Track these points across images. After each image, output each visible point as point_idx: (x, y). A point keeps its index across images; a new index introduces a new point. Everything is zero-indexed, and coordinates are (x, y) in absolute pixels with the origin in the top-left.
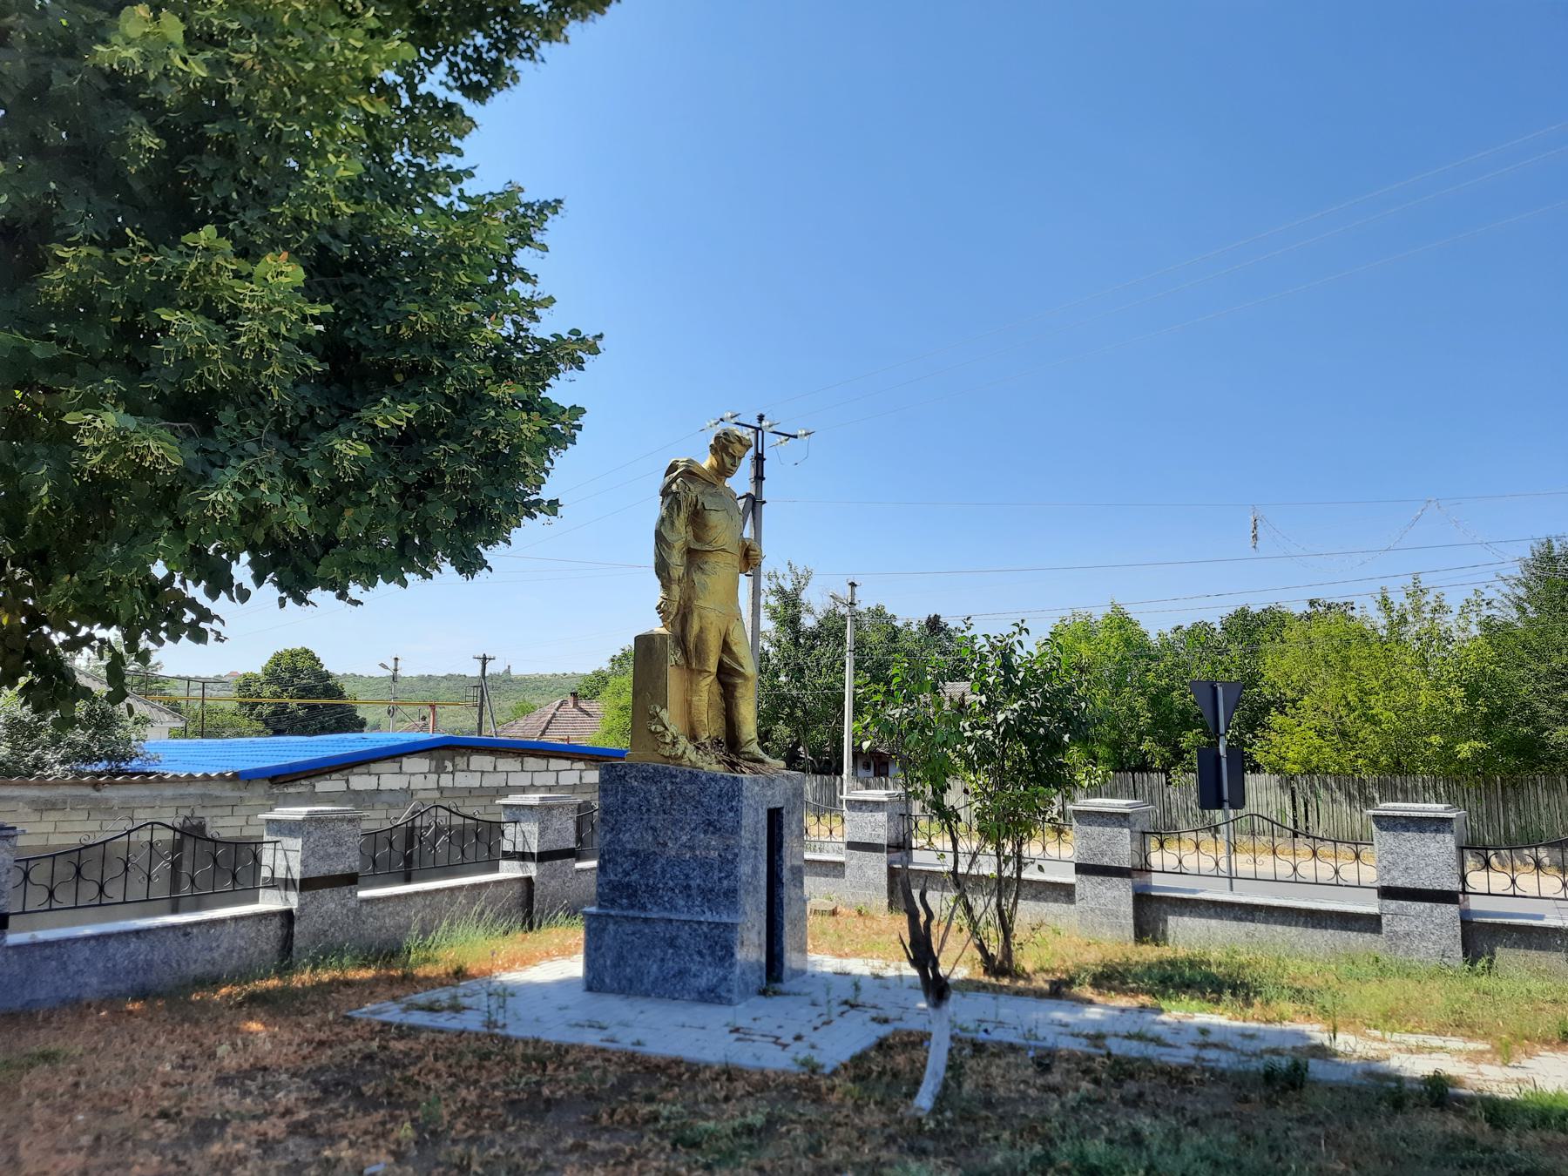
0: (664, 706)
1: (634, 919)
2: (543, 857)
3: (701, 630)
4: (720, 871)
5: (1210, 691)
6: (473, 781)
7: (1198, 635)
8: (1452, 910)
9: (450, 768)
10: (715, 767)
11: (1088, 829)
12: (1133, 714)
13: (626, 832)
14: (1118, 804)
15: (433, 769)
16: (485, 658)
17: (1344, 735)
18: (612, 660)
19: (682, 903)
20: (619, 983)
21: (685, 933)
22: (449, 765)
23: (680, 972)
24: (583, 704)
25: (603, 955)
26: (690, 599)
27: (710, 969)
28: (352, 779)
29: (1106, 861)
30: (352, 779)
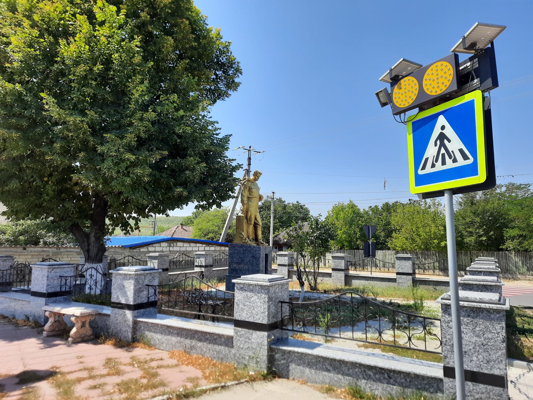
0: (243, 232)
2: (206, 266)
5: (368, 228)
7: (375, 210)
8: (410, 277)
9: (172, 246)
10: (254, 245)
11: (335, 260)
12: (355, 233)
14: (342, 255)
17: (412, 239)
22: (172, 245)
24: (184, 227)
28: (149, 248)
29: (339, 268)
30: (149, 248)
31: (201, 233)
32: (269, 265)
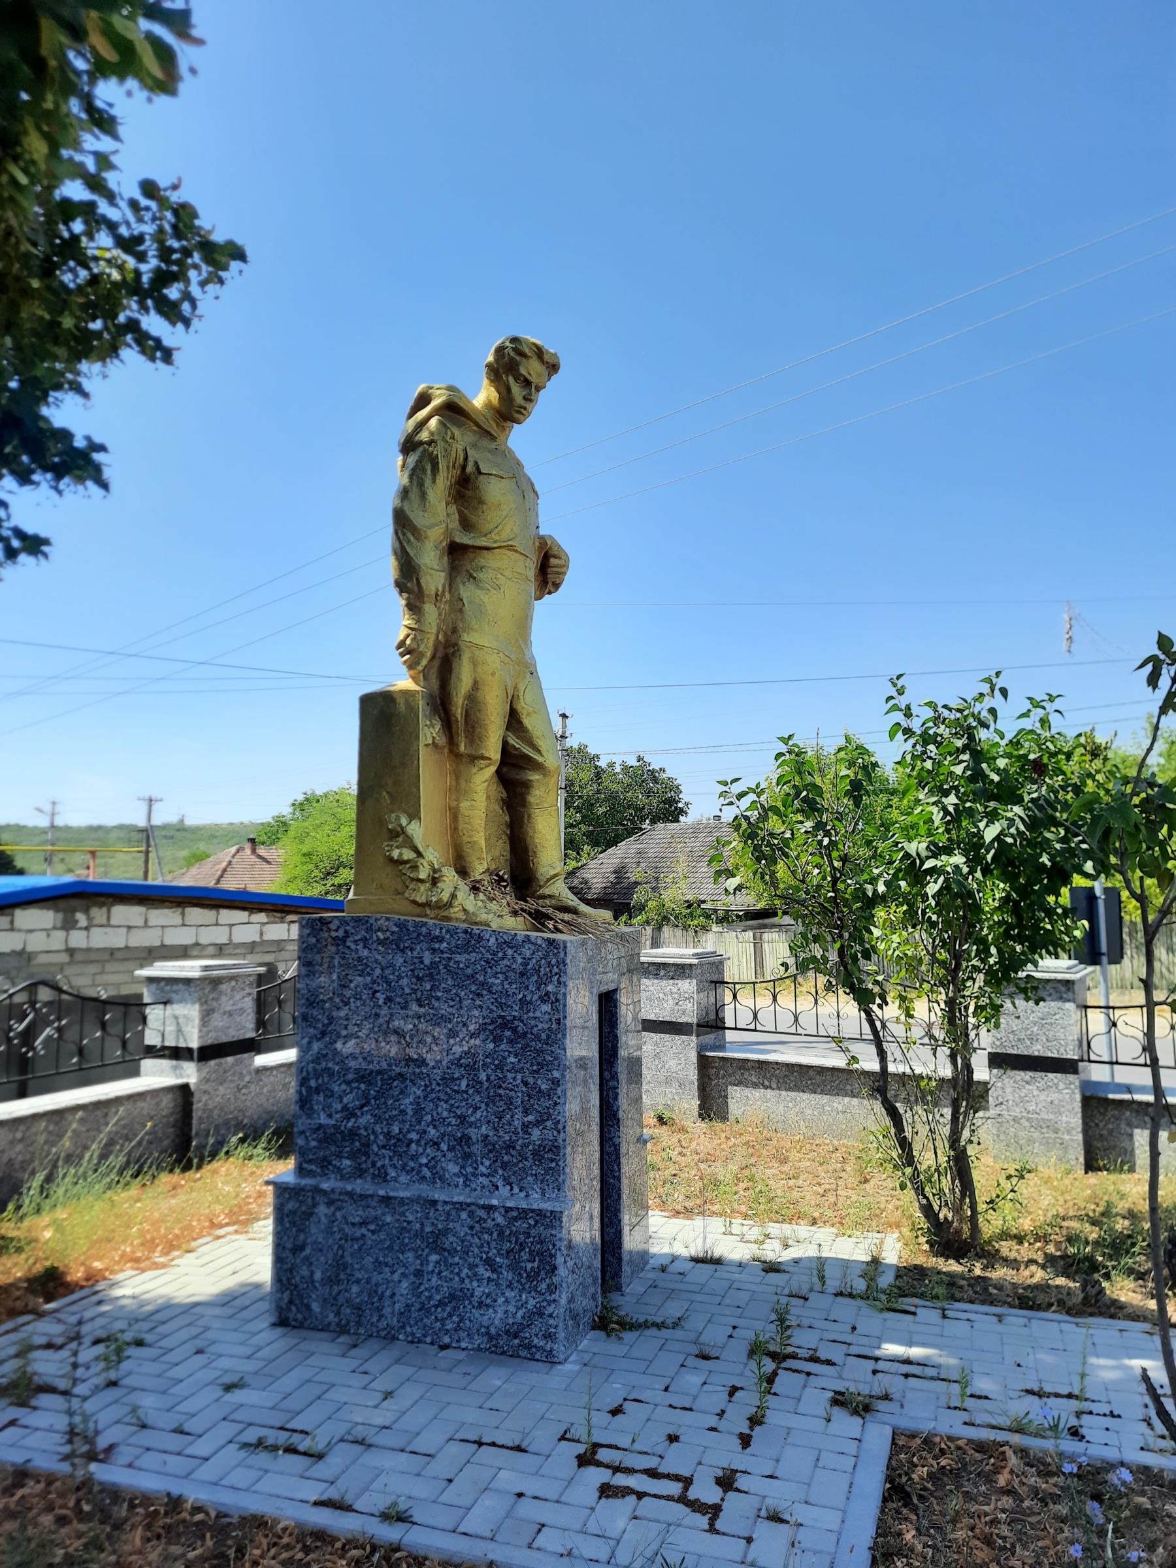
0: (414, 815)
1: (363, 1197)
2: (207, 1053)
3: (476, 686)
4: (526, 1112)
6: (114, 939)
13: (347, 1038)
15: (59, 925)
16: (151, 800)
18: (294, 805)
19: (453, 1168)
20: (338, 1314)
21: (461, 1226)
23: (452, 1297)
25: (308, 1261)
26: (455, 631)
27: (509, 1294)
29: (1037, 1050)
31: (311, 867)
32: (623, 1076)
